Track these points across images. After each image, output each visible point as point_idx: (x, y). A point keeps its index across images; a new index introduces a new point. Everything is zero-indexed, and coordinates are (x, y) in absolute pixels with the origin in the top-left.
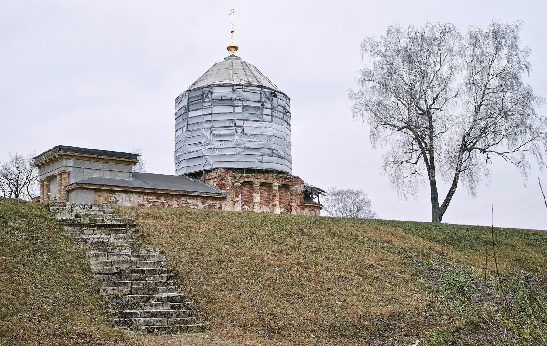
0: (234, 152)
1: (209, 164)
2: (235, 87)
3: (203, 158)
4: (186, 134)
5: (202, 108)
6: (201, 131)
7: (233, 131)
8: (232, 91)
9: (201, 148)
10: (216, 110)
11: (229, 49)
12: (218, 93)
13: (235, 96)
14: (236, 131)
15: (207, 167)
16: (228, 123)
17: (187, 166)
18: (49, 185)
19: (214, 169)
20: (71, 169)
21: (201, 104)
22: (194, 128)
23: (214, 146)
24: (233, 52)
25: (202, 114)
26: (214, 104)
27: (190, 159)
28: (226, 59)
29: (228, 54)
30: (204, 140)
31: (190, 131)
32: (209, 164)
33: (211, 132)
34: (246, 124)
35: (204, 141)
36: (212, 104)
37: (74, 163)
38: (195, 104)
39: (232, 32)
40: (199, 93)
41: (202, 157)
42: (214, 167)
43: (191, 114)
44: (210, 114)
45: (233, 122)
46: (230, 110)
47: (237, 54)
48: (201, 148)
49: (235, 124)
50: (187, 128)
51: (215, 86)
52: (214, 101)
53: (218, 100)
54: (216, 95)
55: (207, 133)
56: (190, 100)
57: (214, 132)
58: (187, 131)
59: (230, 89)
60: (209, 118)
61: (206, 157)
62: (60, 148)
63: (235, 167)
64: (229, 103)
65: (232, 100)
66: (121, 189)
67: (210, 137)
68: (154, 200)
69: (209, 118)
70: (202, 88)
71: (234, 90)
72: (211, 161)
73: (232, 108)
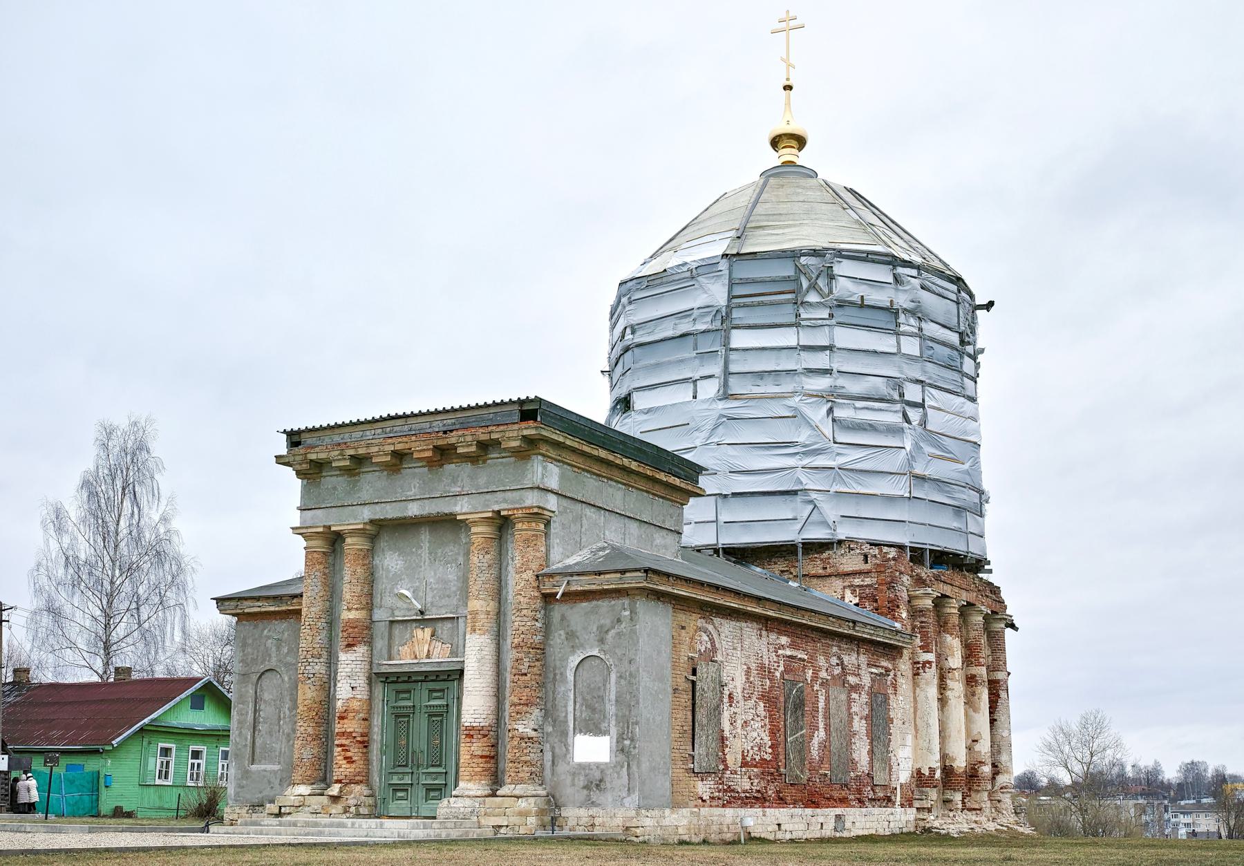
0: (899, 488)
1: (824, 523)
2: (900, 270)
3: (799, 498)
4: (721, 405)
5: (797, 325)
6: (790, 402)
7: (897, 419)
8: (891, 279)
9: (791, 462)
10: (846, 338)
11: (775, 143)
12: (849, 280)
13: (902, 301)
14: (905, 416)
15: (817, 534)
16: (881, 386)
17: (724, 517)
18: (371, 553)
19: (840, 542)
20: (552, 503)
21: (790, 309)
22: (756, 390)
23: (840, 461)
24: (788, 154)
25: (794, 343)
26: (840, 315)
27: (734, 495)
28: (768, 175)
29: (773, 159)
30: (803, 436)
31: (734, 397)
32: (824, 523)
33: (830, 410)
34: (935, 398)
35: (801, 439)
36: (831, 316)
37: (562, 477)
38: (760, 304)
39: (788, 88)
40: (787, 270)
41: (795, 493)
42: (842, 533)
43: (740, 339)
44: (823, 348)
45: (897, 384)
46: (885, 343)
47: (804, 158)
48: (791, 462)
49: (902, 395)
50: (726, 384)
51: (840, 254)
52: (842, 304)
53: (852, 304)
54: (843, 288)
55: (818, 414)
56: (738, 291)
57: (838, 413)
58: (726, 396)
59: (883, 274)
60: (821, 360)
61: (814, 496)
62: (530, 410)
63: (905, 540)
64: (882, 320)
65: (892, 311)
66: (734, 603)
67: (827, 428)
68: (788, 652)
69: (821, 360)
70: (794, 255)
71: (897, 279)
72: (831, 511)
73: (892, 340)
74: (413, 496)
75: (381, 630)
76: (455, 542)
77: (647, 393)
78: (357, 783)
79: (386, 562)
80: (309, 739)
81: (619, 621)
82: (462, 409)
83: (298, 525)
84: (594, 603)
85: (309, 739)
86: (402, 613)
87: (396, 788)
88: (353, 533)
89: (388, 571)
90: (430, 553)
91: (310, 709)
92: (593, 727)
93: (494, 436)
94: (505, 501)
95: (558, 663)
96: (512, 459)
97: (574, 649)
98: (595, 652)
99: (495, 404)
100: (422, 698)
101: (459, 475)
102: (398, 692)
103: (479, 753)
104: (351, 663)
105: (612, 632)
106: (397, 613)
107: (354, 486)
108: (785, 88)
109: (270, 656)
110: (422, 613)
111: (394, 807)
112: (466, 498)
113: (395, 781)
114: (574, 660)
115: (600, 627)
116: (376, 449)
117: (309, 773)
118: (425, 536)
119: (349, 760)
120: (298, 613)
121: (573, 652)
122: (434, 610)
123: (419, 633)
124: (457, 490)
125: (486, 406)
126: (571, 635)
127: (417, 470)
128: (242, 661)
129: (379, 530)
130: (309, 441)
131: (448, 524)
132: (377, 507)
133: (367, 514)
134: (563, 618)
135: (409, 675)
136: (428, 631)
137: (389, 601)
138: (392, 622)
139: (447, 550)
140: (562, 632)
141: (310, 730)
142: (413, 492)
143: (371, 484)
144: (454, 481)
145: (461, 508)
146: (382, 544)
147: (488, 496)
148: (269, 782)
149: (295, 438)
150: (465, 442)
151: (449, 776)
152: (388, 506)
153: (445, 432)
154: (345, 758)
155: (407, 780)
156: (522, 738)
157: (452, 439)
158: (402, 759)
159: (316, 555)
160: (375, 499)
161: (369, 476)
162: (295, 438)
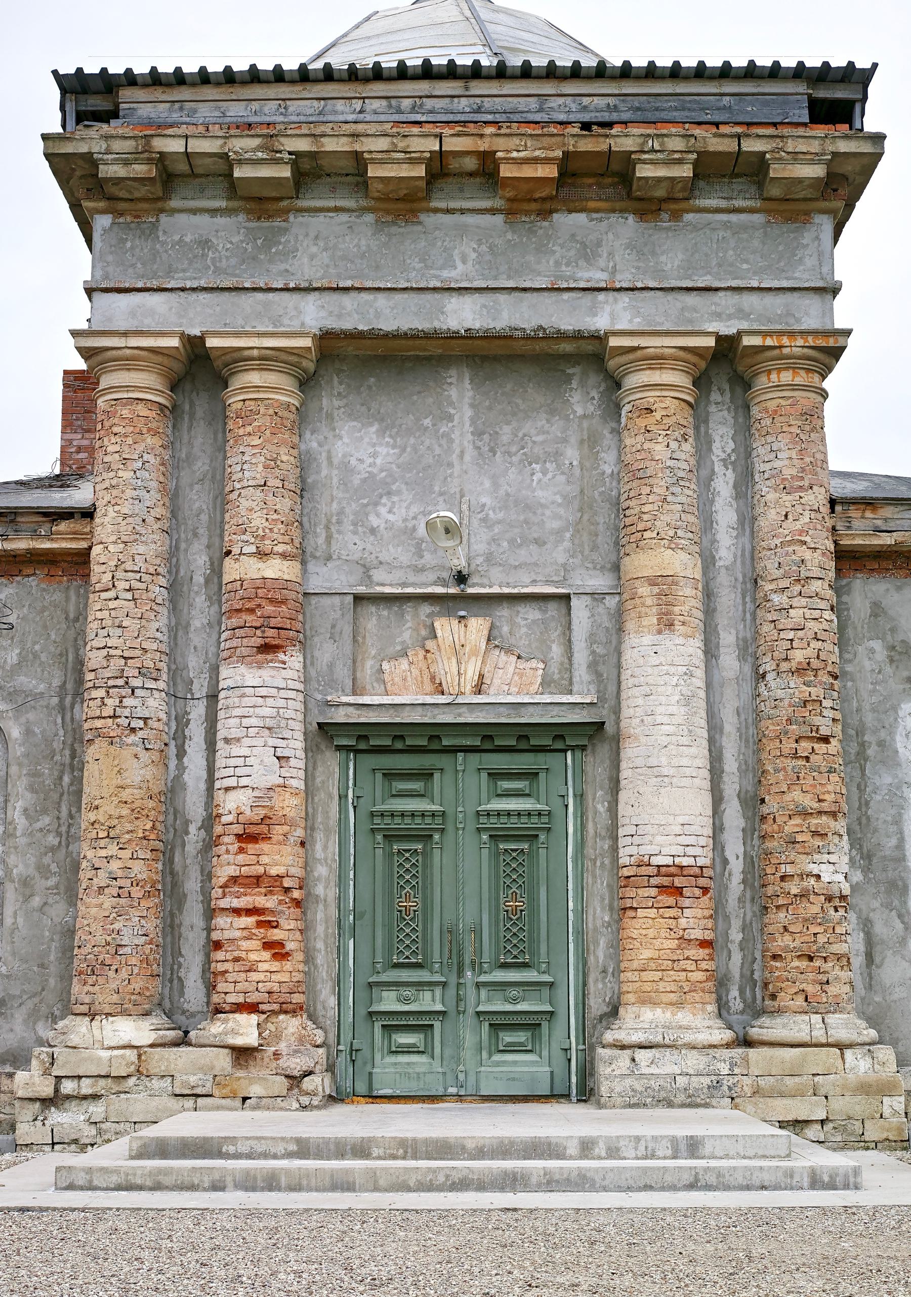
74: (460, 276)
75: (330, 613)
76: (552, 412)
77: (227, 294)
78: (293, 1012)
79: (340, 448)
80: (137, 892)
82: (651, 72)
83: (85, 326)
85: (137, 892)
86: (398, 576)
87: (394, 1023)
88: (268, 360)
89: (346, 468)
90: (478, 434)
91: (138, 813)
93: (751, 146)
94: (741, 314)
95: (869, 719)
96: (758, 218)
99: (751, 72)
100: (464, 791)
101: (610, 241)
102: (495, 776)
103: (697, 934)
106: (378, 575)
107: (269, 243)
110: (461, 578)
111: (388, 1071)
112: (625, 298)
113: (389, 1002)
116: (383, 144)
117: (137, 985)
118: (460, 393)
119: (277, 950)
120: (80, 562)
122: (496, 573)
123: (445, 627)
124: (599, 277)
125: (726, 72)
127: (469, 219)
129: (348, 360)
130: (145, 111)
131: (591, 359)
132: (348, 301)
133: (313, 315)
134: (877, 610)
135: (434, 731)
136: (477, 627)
137: (350, 544)
138: (358, 599)
139: (528, 427)
140: (877, 645)
141: (139, 869)
142: (459, 273)
143: (324, 238)
144: (588, 253)
145: (609, 317)
146: (328, 400)
147: (692, 299)
149: (90, 96)
151: (561, 992)
152: (381, 300)
154: (268, 945)
155: (428, 1002)
156: (829, 899)
158: (400, 937)
159: (142, 410)
160: (324, 277)
161: (319, 222)
162: (90, 96)
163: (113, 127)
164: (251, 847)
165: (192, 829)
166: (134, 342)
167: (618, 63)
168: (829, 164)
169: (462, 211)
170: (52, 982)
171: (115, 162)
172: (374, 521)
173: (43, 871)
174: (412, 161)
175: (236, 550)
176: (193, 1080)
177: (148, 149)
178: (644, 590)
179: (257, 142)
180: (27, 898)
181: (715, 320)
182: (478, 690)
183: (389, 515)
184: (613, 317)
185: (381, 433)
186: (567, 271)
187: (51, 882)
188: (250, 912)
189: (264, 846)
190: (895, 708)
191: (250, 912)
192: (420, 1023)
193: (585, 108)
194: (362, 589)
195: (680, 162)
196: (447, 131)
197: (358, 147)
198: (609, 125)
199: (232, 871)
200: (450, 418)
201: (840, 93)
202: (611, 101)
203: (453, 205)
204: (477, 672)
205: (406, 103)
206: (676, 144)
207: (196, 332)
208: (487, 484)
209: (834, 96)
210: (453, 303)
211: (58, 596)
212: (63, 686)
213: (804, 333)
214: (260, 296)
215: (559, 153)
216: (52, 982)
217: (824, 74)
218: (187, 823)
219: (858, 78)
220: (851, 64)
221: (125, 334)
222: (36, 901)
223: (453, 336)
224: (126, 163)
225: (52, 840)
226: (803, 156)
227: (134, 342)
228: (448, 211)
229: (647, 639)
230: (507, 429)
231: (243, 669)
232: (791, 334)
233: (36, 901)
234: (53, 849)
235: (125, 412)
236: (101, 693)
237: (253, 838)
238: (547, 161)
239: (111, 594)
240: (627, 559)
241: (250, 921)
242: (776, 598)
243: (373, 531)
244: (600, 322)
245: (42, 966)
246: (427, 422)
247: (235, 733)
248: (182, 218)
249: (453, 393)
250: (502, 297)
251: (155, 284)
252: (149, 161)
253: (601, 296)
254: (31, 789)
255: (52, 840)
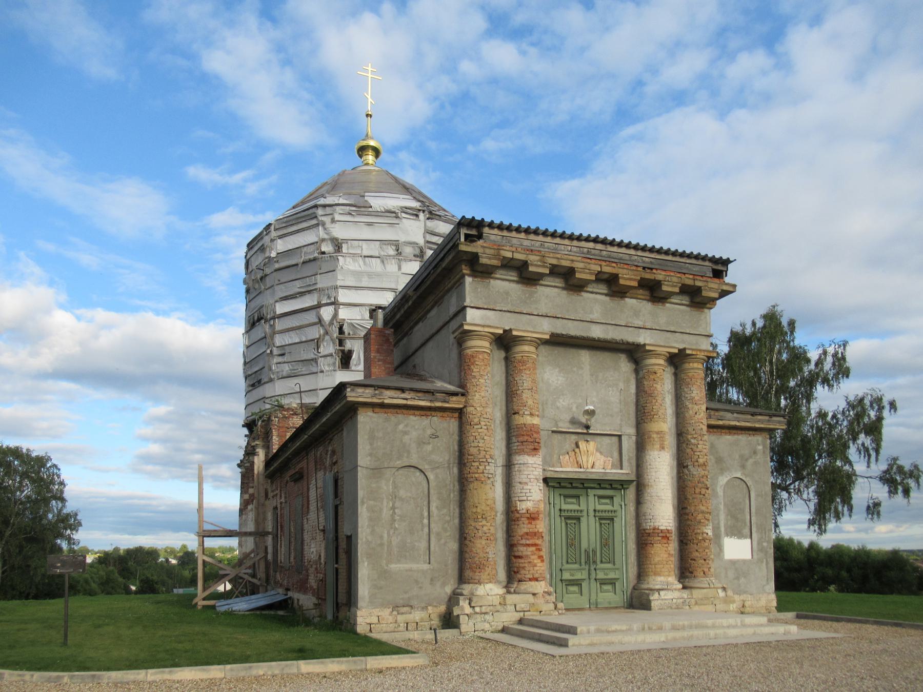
79: (546, 376)
81: (755, 453)
84: (736, 437)
90: (592, 375)
92: (735, 532)
93: (698, 284)
97: (722, 471)
98: (739, 475)
100: (590, 503)
104: (531, 469)
105: (751, 461)
108: (371, 116)
109: (409, 452)
113: (567, 576)
114: (723, 480)
115: (741, 456)
118: (585, 356)
121: (722, 474)
126: (719, 460)
127: (598, 296)
128: (370, 455)
132: (559, 322)
144: (636, 314)
145: (643, 338)
147: (669, 334)
148: (417, 582)
150: (670, 282)
153: (644, 268)
157: (660, 276)
163: (481, 242)
164: (533, 522)
165: (499, 514)
166: (487, 330)
167: (544, 229)
168: (596, 275)
169: (596, 293)
170: (450, 571)
171: (486, 258)
172: (559, 405)
173: (445, 530)
174: (591, 274)
175: (521, 412)
176: (523, 606)
177: (499, 255)
178: (655, 436)
179: (538, 258)
180: (439, 540)
181: (675, 344)
182: (592, 467)
183: (563, 402)
184: (645, 339)
185: (560, 372)
186: (630, 320)
187: (448, 534)
188: (533, 545)
189: (538, 522)
190: (717, 478)
191: (533, 545)
192: (577, 583)
193: (644, 262)
194: (555, 429)
195: (675, 286)
196: (604, 263)
197: (573, 265)
198: (652, 269)
199: (525, 530)
200: (582, 368)
201: (720, 267)
202: (653, 260)
203: (595, 290)
204: (596, 461)
205: (586, 250)
206: (675, 279)
207: (507, 328)
208: (595, 394)
209: (719, 267)
210: (594, 327)
211: (445, 425)
212: (449, 460)
213: (704, 351)
214: (528, 316)
215: (639, 278)
216: (450, 571)
217: (713, 260)
218: (496, 512)
219: (726, 262)
220: (473, 218)
221: (483, 326)
222: (443, 541)
223: (593, 340)
224: (490, 259)
225: (447, 518)
226: (710, 288)
227: (487, 330)
228: (592, 293)
229: (656, 453)
230: (601, 374)
231: (526, 457)
232: (700, 350)
233: (443, 541)
234: (448, 522)
235: (481, 357)
236: (477, 464)
237: (534, 519)
238: (634, 280)
239: (479, 426)
240: (517, 416)
241: (534, 548)
242: (693, 441)
243: (558, 408)
244: (641, 340)
245: (446, 566)
246: (575, 369)
247: (524, 480)
248: (499, 282)
249: (583, 359)
250: (609, 327)
251: (491, 307)
252: (499, 259)
253: (641, 330)
254: (439, 499)
255: (447, 518)
